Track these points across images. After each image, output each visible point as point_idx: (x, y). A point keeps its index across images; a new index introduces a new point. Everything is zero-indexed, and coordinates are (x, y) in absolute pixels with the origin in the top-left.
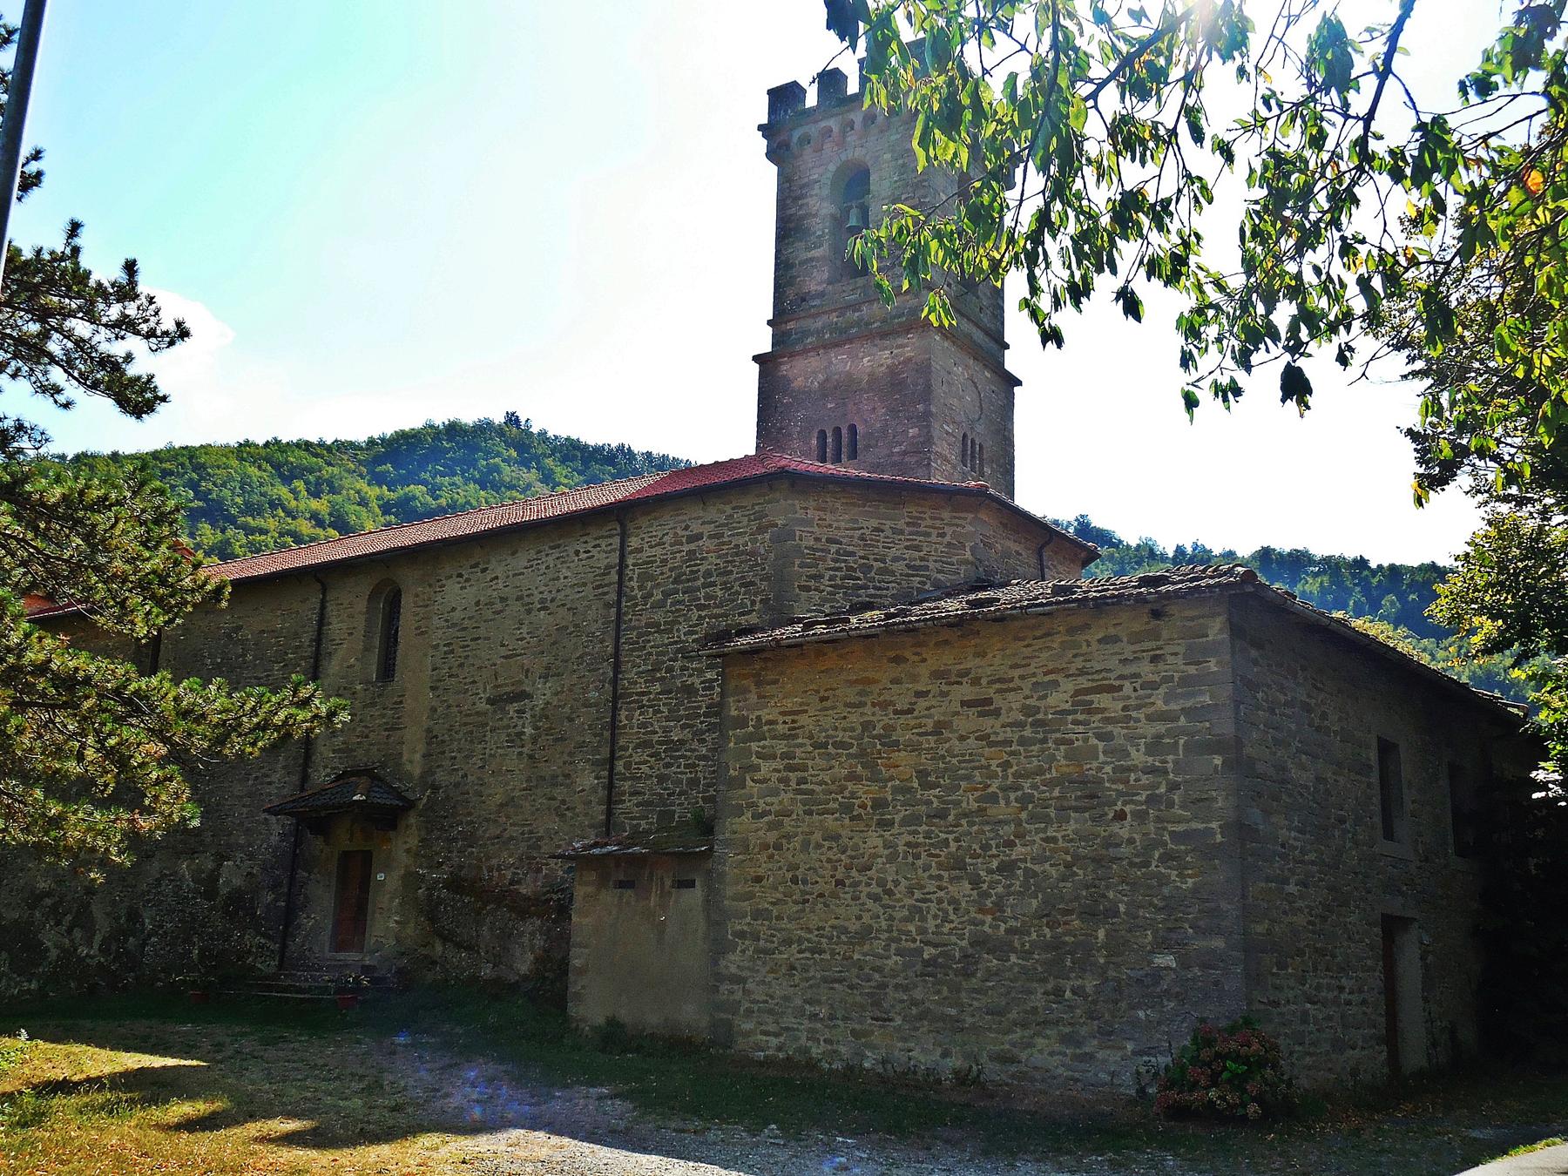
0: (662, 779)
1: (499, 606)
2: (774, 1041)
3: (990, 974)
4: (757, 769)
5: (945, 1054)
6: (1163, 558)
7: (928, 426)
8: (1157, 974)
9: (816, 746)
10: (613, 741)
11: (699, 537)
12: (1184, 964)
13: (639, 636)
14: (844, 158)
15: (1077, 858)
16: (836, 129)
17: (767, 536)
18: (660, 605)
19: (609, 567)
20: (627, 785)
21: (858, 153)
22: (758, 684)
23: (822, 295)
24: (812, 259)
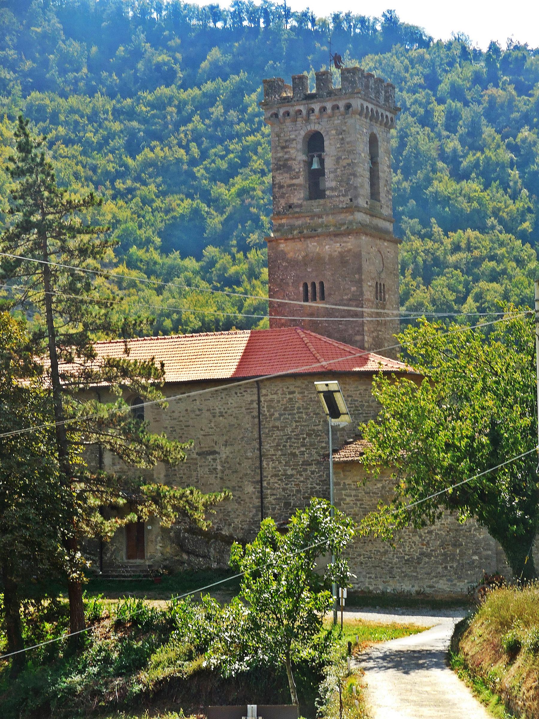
0: (284, 489)
1: (198, 413)
2: (357, 586)
3: (426, 563)
5: (413, 586)
6: (477, 54)
7: (361, 287)
8: (473, 561)
9: (366, 493)
10: (261, 474)
11: (293, 392)
12: (481, 558)
14: (309, 129)
15: (450, 529)
16: (304, 112)
18: (279, 419)
19: (252, 401)
20: (269, 491)
21: (317, 128)
22: (343, 471)
23: (300, 206)
24: (293, 185)
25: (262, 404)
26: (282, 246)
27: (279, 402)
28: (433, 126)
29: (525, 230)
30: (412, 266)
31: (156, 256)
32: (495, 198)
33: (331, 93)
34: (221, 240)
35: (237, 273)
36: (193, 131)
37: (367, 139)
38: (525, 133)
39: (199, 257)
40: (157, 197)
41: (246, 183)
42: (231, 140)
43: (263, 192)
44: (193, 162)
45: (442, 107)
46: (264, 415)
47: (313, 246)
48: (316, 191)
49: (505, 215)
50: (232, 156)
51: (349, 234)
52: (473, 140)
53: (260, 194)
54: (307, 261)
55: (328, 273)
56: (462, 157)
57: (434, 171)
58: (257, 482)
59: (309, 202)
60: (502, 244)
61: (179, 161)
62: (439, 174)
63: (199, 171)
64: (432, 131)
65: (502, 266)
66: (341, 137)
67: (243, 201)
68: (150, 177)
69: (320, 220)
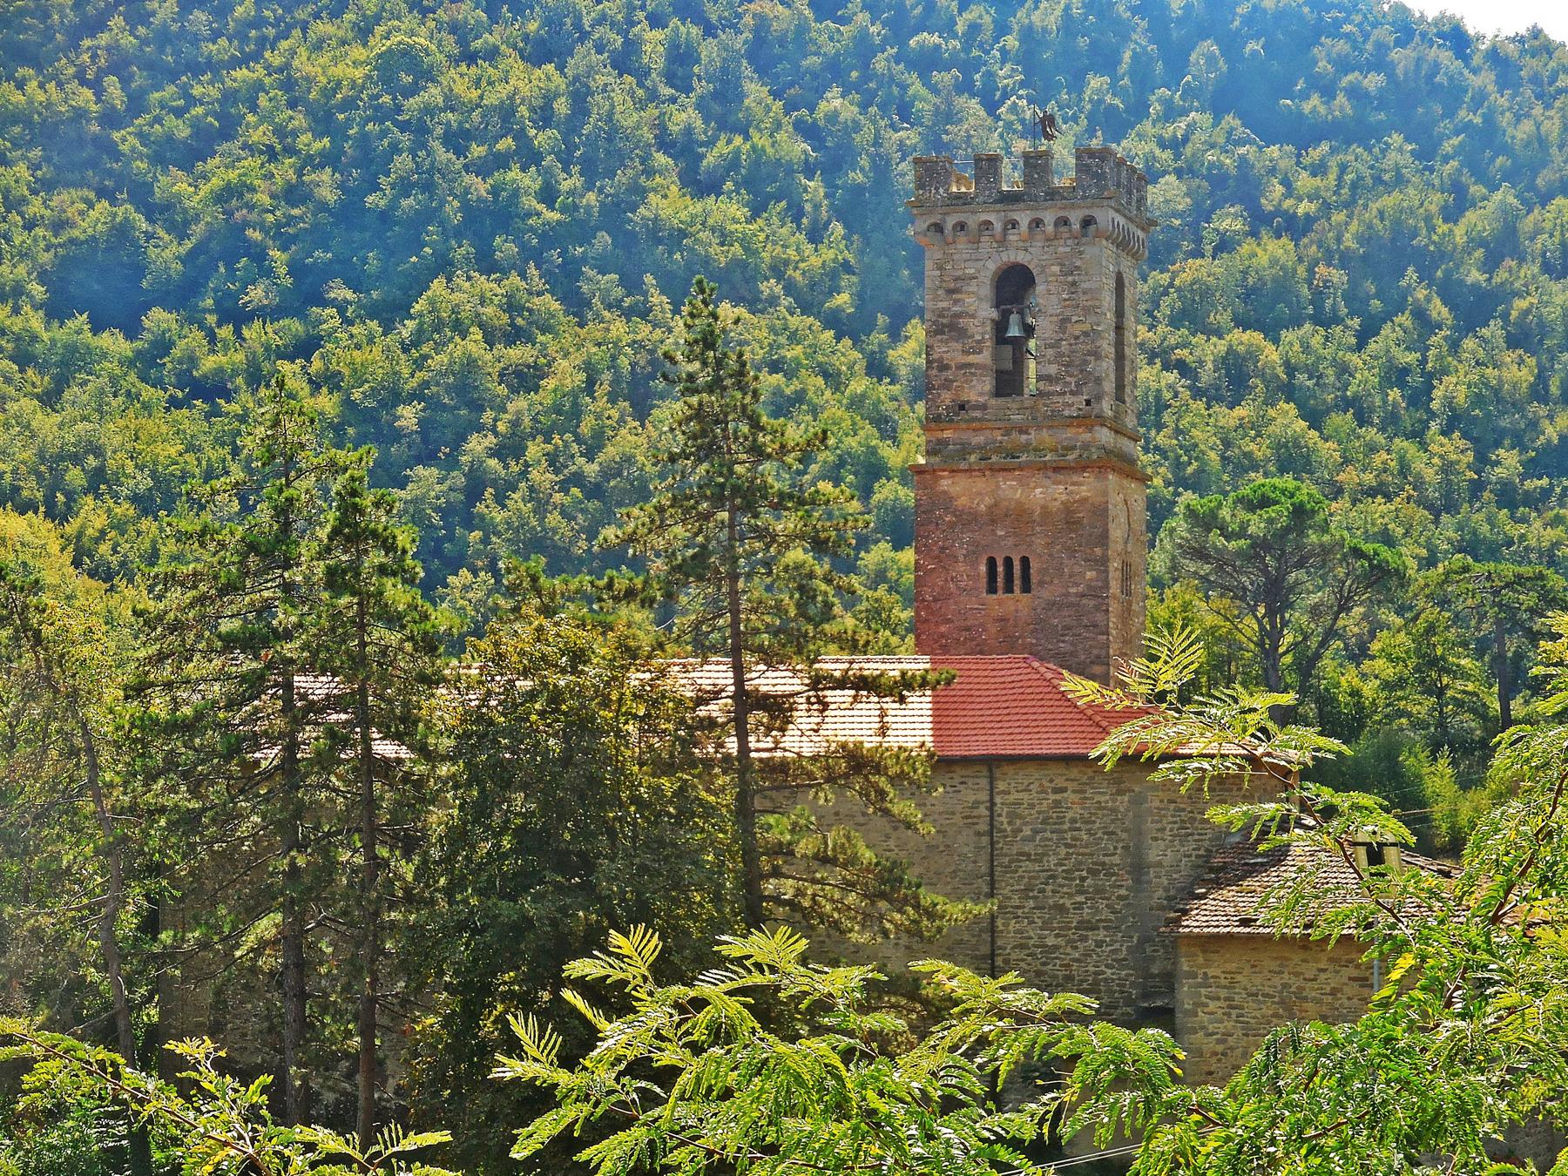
4: (1207, 1005)
10: (993, 942)
11: (1063, 790)
13: (1011, 862)
14: (1005, 259)
16: (998, 226)
17: (1126, 798)
18: (1031, 839)
19: (976, 804)
21: (1022, 258)
22: (1204, 951)
23: (984, 407)
24: (970, 365)
25: (997, 809)
26: (945, 484)
27: (1032, 806)
28: (642, 75)
29: (839, 310)
30: (607, 376)
31: (36, 322)
32: (777, 238)
33: (1053, 194)
34: (181, 296)
35: (220, 370)
36: (108, 49)
37: (1112, 283)
38: (834, 102)
39: (132, 331)
40: (34, 192)
41: (233, 175)
42: (195, 76)
43: (273, 196)
44: (111, 119)
45: (658, 34)
46: (1001, 831)
47: (1010, 489)
48: (1008, 383)
49: (797, 275)
50: (199, 110)
51: (1084, 469)
52: (724, 108)
53: (265, 199)
54: (994, 516)
55: (1040, 541)
56: (702, 144)
57: (649, 172)
58: (984, 957)
59: (1001, 401)
60: (794, 338)
61: (80, 114)
62: (658, 179)
63: (126, 139)
64: (640, 85)
65: (795, 385)
66: (1070, 279)
67: (229, 213)
68: (16, 146)
69: (1024, 437)
